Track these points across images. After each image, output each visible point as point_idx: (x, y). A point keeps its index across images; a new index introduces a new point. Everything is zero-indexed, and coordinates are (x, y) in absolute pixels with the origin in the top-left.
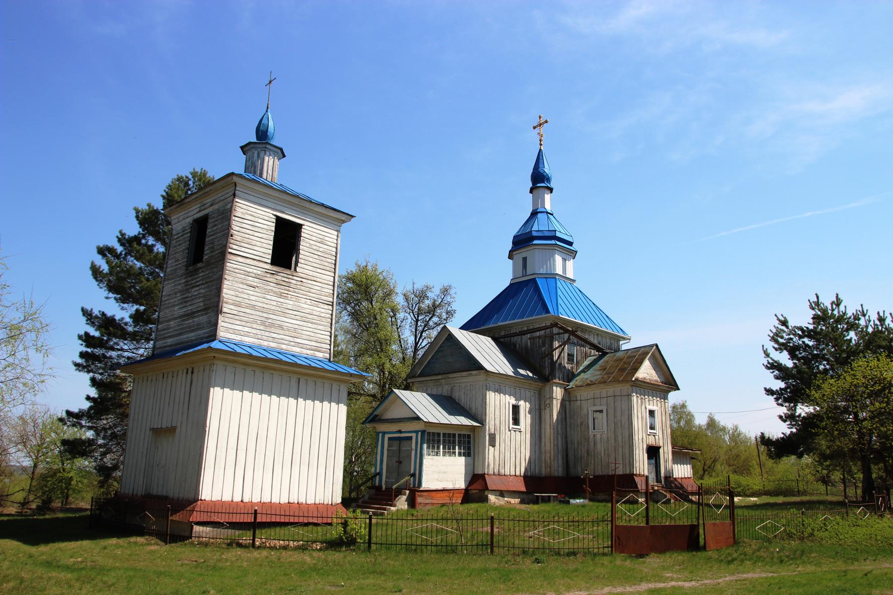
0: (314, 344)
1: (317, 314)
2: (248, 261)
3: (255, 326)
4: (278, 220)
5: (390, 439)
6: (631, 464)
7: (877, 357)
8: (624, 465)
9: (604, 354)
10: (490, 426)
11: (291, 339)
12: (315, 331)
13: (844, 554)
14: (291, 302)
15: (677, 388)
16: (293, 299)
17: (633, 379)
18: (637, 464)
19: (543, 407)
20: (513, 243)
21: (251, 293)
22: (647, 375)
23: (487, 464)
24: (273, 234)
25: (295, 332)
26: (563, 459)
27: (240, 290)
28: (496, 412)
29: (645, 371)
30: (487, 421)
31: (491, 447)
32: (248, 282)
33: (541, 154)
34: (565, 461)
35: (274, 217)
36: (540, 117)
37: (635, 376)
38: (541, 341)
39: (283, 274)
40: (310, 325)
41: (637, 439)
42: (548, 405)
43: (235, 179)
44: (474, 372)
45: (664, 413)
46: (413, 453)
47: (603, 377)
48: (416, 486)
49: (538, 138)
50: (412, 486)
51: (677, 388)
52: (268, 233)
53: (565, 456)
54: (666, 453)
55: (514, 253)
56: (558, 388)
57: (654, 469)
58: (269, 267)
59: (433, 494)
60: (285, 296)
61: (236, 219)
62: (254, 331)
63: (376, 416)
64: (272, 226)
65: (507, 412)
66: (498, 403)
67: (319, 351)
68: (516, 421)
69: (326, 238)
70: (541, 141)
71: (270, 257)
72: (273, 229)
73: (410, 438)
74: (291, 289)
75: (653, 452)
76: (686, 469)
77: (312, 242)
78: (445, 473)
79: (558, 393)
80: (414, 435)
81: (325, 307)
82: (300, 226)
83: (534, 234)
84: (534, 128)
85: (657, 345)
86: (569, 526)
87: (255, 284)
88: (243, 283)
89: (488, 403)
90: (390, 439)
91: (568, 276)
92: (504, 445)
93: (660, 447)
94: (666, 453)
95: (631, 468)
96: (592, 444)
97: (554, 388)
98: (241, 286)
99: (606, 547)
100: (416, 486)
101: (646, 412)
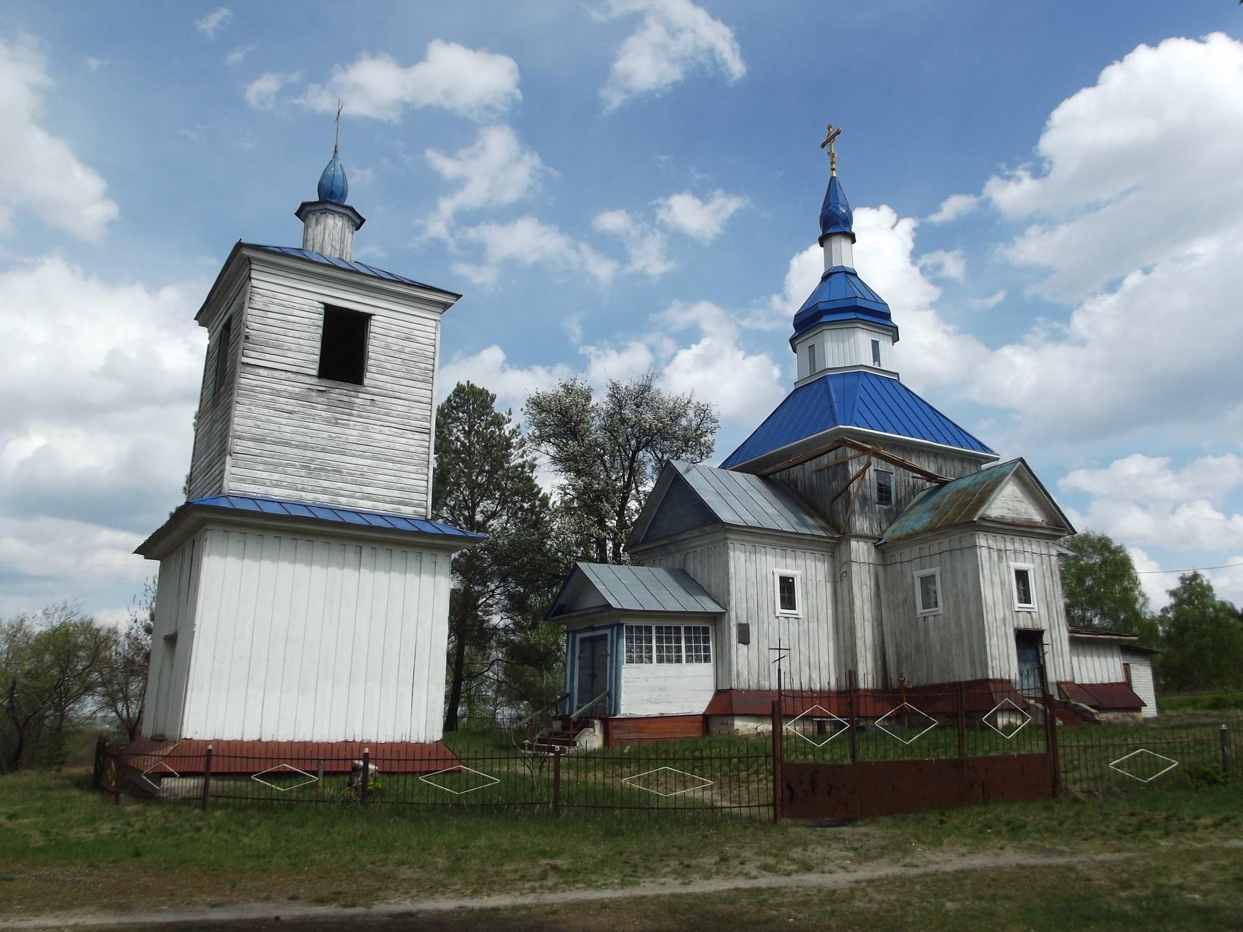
0: (397, 493)
1: (401, 448)
2: (276, 374)
3: (290, 470)
4: (328, 307)
5: (582, 640)
8: (973, 664)
9: (943, 484)
10: (739, 612)
11: (355, 488)
12: (398, 473)
13: (60, 827)
14: (355, 432)
16: (357, 428)
19: (838, 578)
20: (795, 326)
21: (284, 421)
24: (321, 331)
25: (362, 478)
26: (875, 659)
27: (263, 418)
28: (749, 590)
30: (733, 603)
32: (278, 406)
34: (879, 662)
35: (322, 306)
37: (980, 513)
38: (830, 472)
39: (339, 392)
40: (390, 465)
43: (246, 252)
44: (708, 529)
47: (931, 521)
48: (613, 712)
49: (828, 159)
52: (310, 330)
53: (879, 656)
54: (1057, 638)
58: (315, 381)
60: (344, 425)
61: (255, 312)
62: (290, 479)
63: (563, 606)
64: (319, 320)
65: (770, 589)
67: (407, 504)
69: (416, 333)
70: (832, 163)
71: (316, 366)
72: (321, 323)
74: (354, 412)
75: (1029, 641)
76: (1112, 668)
77: (390, 340)
80: (608, 632)
81: (416, 437)
82: (364, 319)
83: (822, 307)
84: (823, 146)
85: (1022, 460)
87: (290, 408)
88: (268, 408)
89: (732, 570)
90: (582, 640)
91: (883, 367)
94: (1057, 638)
95: (984, 669)
96: (922, 633)
97: (854, 544)
98: (266, 411)
99: (764, 805)
100: (613, 712)
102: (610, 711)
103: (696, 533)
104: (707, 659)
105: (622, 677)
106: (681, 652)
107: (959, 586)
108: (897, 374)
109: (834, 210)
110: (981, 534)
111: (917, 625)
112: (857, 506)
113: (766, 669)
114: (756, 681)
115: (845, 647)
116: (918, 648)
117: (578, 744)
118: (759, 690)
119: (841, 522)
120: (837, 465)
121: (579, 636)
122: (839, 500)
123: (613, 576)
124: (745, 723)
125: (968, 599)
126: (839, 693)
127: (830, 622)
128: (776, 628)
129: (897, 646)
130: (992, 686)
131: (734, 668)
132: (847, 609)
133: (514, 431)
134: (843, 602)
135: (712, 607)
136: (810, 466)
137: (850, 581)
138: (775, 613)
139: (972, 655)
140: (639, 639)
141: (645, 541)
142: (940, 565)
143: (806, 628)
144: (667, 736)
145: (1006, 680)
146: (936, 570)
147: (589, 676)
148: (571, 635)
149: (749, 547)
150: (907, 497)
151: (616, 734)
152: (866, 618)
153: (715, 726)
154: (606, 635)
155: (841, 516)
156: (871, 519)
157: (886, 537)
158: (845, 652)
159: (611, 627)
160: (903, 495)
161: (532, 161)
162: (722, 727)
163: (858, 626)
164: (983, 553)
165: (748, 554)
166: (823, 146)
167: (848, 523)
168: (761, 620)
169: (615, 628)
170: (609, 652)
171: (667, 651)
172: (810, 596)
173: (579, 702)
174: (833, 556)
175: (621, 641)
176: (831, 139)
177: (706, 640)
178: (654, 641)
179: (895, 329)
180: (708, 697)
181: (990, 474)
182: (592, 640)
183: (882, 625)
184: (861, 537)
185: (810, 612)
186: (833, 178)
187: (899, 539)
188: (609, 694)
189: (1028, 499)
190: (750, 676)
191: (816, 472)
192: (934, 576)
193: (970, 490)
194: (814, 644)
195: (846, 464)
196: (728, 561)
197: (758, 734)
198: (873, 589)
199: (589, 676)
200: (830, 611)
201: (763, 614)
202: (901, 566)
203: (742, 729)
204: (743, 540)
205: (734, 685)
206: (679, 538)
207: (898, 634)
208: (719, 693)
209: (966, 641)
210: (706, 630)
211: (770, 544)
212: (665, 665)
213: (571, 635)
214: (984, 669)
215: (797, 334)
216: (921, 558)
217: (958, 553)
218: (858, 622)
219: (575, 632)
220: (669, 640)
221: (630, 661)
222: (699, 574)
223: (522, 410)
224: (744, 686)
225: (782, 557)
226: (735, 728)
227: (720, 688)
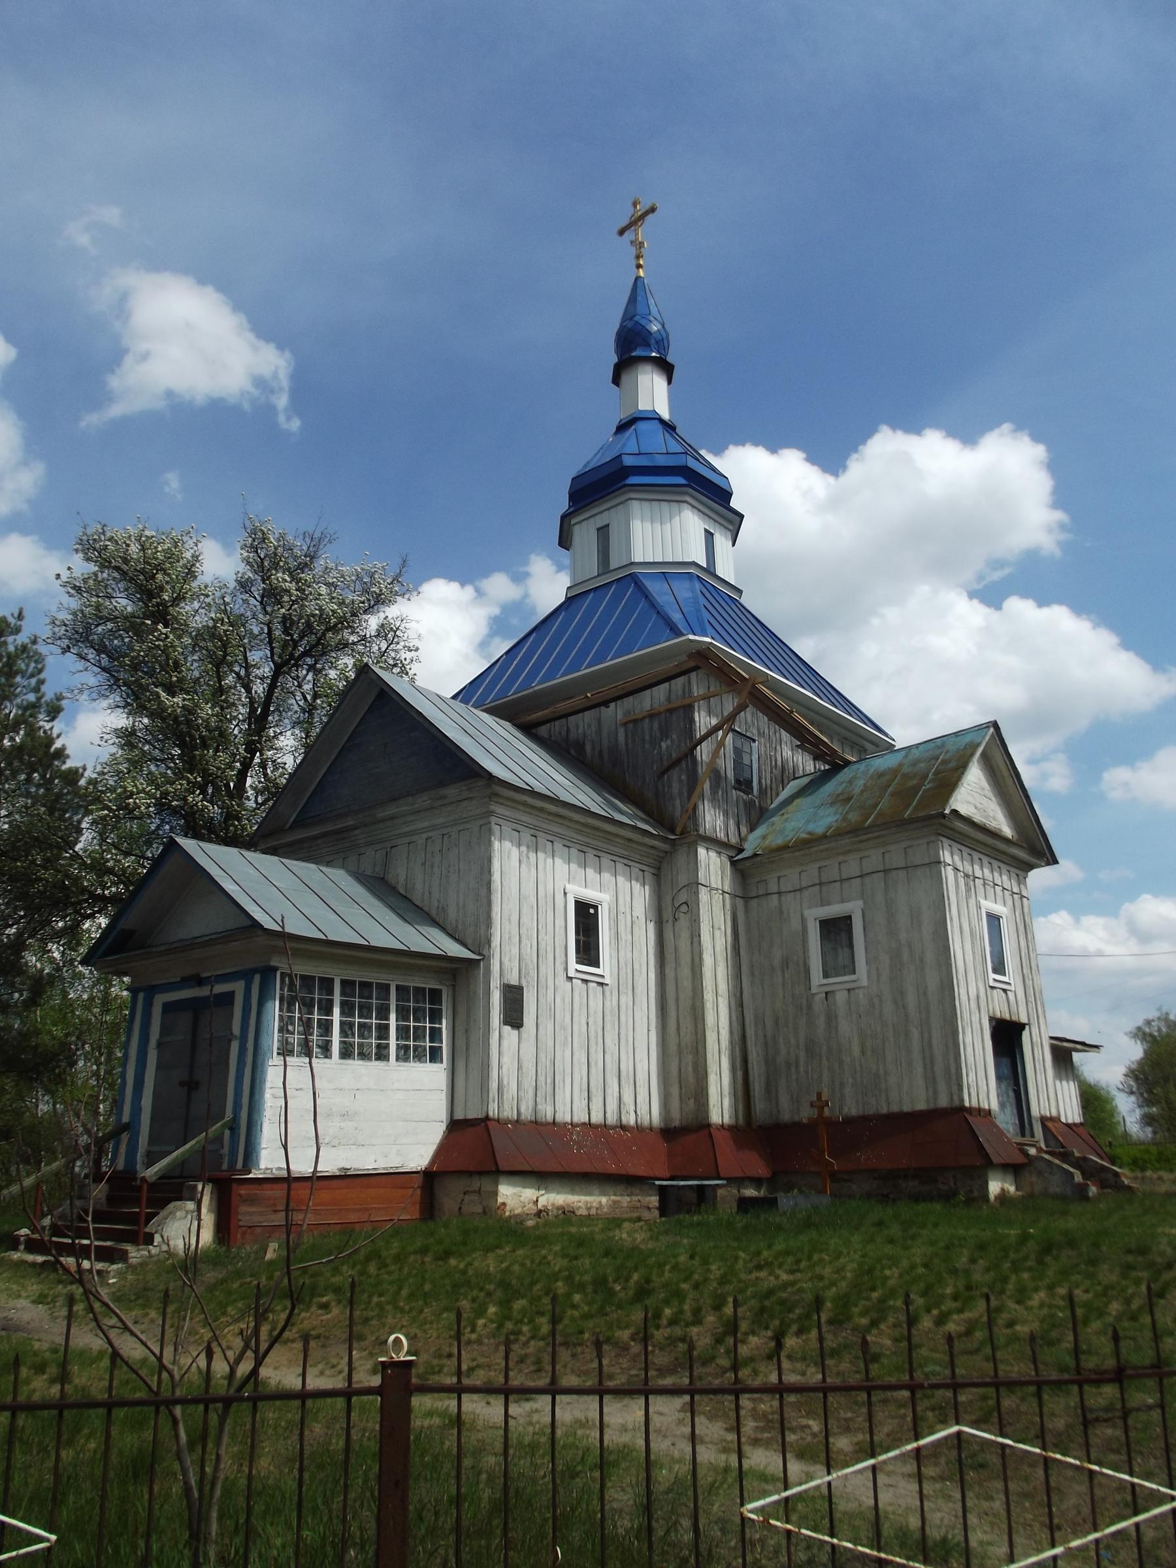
5: (168, 1008)
6: (955, 1077)
7: (71, 1301)
8: (931, 1081)
10: (506, 960)
15: (1053, 860)
17: (947, 811)
18: (972, 1076)
22: (974, 810)
23: (494, 1085)
28: (524, 920)
29: (970, 799)
30: (496, 942)
31: (507, 1028)
33: (640, 292)
34: (740, 1074)
36: (635, 204)
38: (656, 725)
41: (964, 997)
42: (684, 908)
44: (451, 792)
45: (1021, 929)
46: (235, 1046)
48: (239, 1165)
49: (633, 251)
50: (225, 1166)
51: (1053, 860)
53: (738, 1064)
55: (573, 522)
56: (713, 854)
57: (1012, 1094)
59: (372, 1179)
65: (560, 922)
66: (528, 889)
68: (588, 951)
70: (638, 257)
73: (229, 998)
78: (345, 1115)
79: (139, 1553)
80: (238, 987)
83: (628, 461)
84: (621, 232)
85: (995, 725)
86: (1087, 1421)
89: (496, 877)
90: (168, 1008)
92: (550, 1027)
93: (1022, 1027)
95: (955, 1088)
96: (821, 1021)
97: (702, 852)
100: (239, 1165)
101: (980, 919)
102: (233, 1162)
103: (423, 800)
104: (435, 1055)
105: (268, 1085)
106: (387, 1038)
107: (903, 936)
108: (740, 592)
109: (643, 322)
110: (946, 842)
111: (810, 1007)
112: (707, 786)
113: (549, 1080)
114: (531, 1103)
115: (679, 1045)
116: (811, 1048)
117: (157, 1239)
118: (536, 1122)
119: (678, 813)
120: (671, 711)
121: (160, 1000)
122: (675, 773)
123: (252, 871)
124: (517, 1190)
125: (922, 960)
126: (668, 1133)
127: (652, 994)
128: (568, 1000)
129: (766, 1044)
130: (490, 1124)
131: (494, 1074)
132: (686, 972)
133: (24, 648)
134: (677, 959)
135: (454, 949)
136: (615, 713)
137: (695, 922)
138: (566, 969)
139: (929, 1062)
140: (308, 1006)
141: (299, 823)
142: (862, 898)
143: (615, 1003)
144: (353, 1217)
145: (975, 1109)
146: (854, 908)
147: (182, 1084)
148: (141, 996)
149: (526, 836)
150: (774, 786)
151: (247, 1214)
152: (720, 992)
153: (450, 1198)
154: (231, 995)
155: (678, 802)
156: (726, 814)
157: (749, 848)
158: (680, 1053)
159: (246, 975)
160: (769, 782)
161: (39, 468)
162: (467, 1198)
163: (709, 1005)
164: (949, 874)
165: (524, 849)
166: (621, 232)
167: (693, 815)
168: (542, 979)
169: (257, 979)
170: (236, 1029)
171: (361, 1036)
172: (622, 943)
173: (152, 1140)
174: (658, 876)
175: (269, 1005)
176: (636, 222)
177: (436, 1016)
178: (336, 1011)
179: (738, 519)
180: (435, 1133)
181: (943, 745)
182: (196, 1007)
183: (742, 1007)
184: (713, 842)
185: (622, 973)
186: (638, 278)
187: (784, 848)
188: (233, 1127)
189: (995, 796)
190: (521, 1093)
191: (625, 724)
192: (849, 918)
193: (905, 770)
194: (627, 1036)
195: (688, 709)
196: (490, 860)
197: (539, 1213)
198: (729, 939)
199: (182, 1084)
200: (652, 976)
201: (546, 969)
202: (780, 900)
203: (511, 1203)
204: (518, 822)
205: (493, 1111)
206: (381, 814)
207: (769, 1022)
208: (455, 1126)
209: (915, 1034)
210: (435, 996)
211: (561, 837)
212: (356, 1064)
213: (141, 996)
214: (955, 1088)
215: (572, 509)
216: (820, 884)
217: (902, 874)
218: (709, 996)
219: (151, 991)
220: (365, 1011)
221: (286, 1051)
222: (419, 886)
223: (58, 576)
224: (509, 1112)
225: (579, 865)
226: (500, 1200)
227: (459, 1116)
